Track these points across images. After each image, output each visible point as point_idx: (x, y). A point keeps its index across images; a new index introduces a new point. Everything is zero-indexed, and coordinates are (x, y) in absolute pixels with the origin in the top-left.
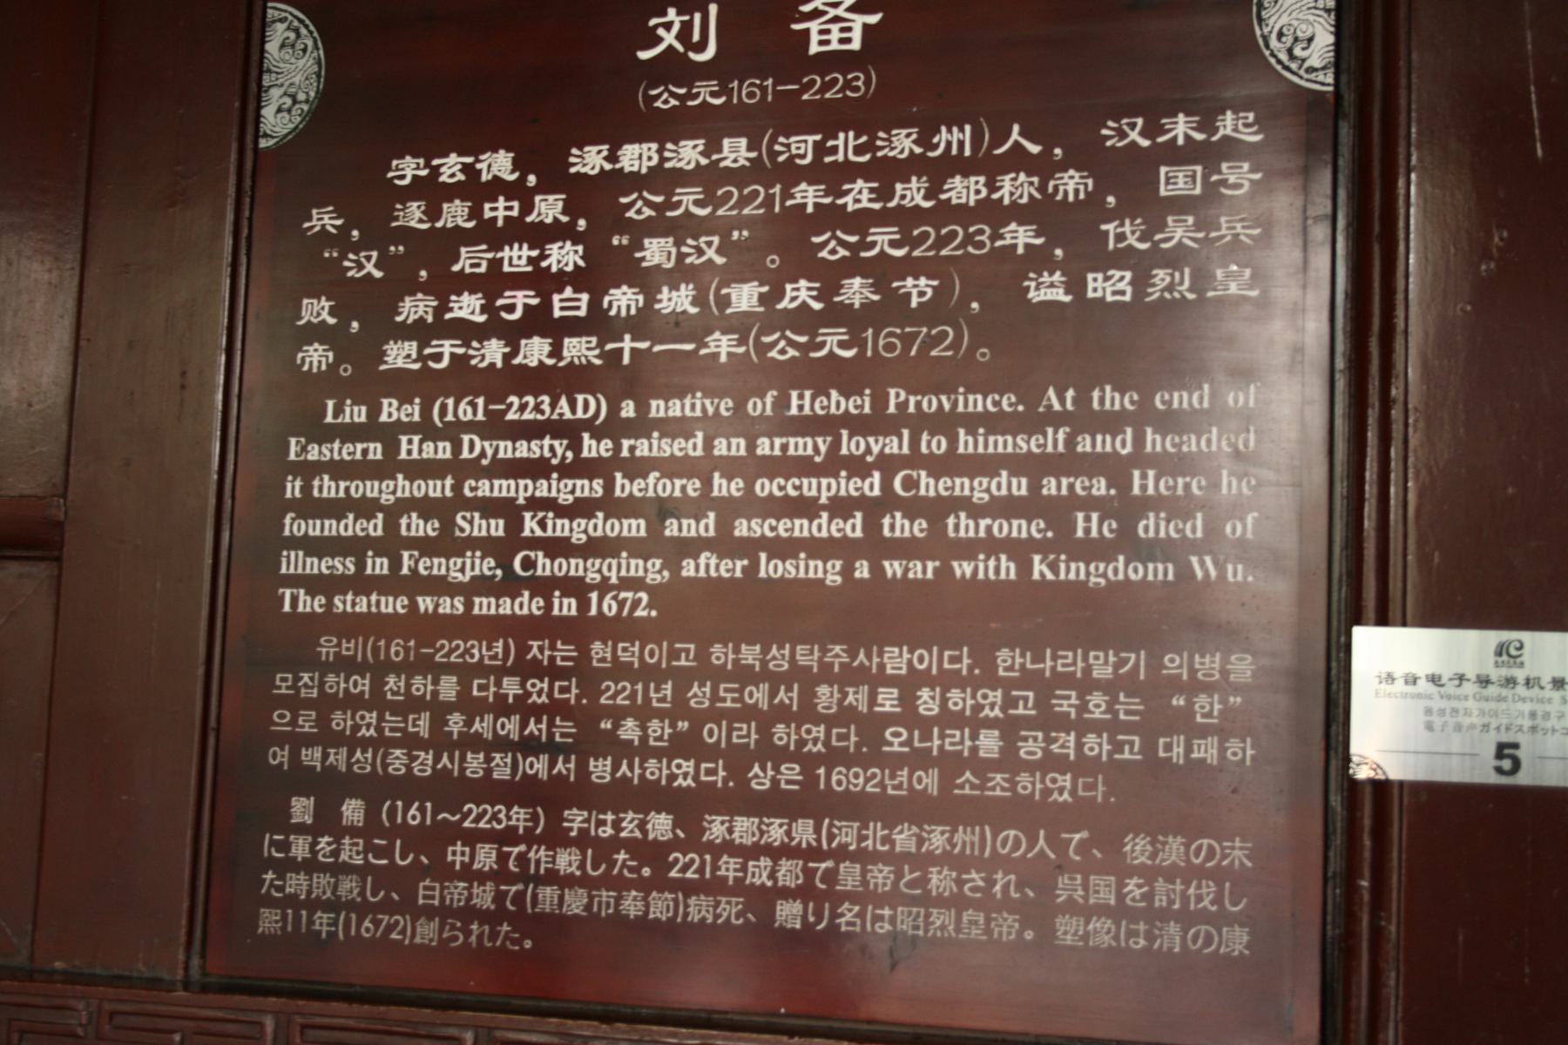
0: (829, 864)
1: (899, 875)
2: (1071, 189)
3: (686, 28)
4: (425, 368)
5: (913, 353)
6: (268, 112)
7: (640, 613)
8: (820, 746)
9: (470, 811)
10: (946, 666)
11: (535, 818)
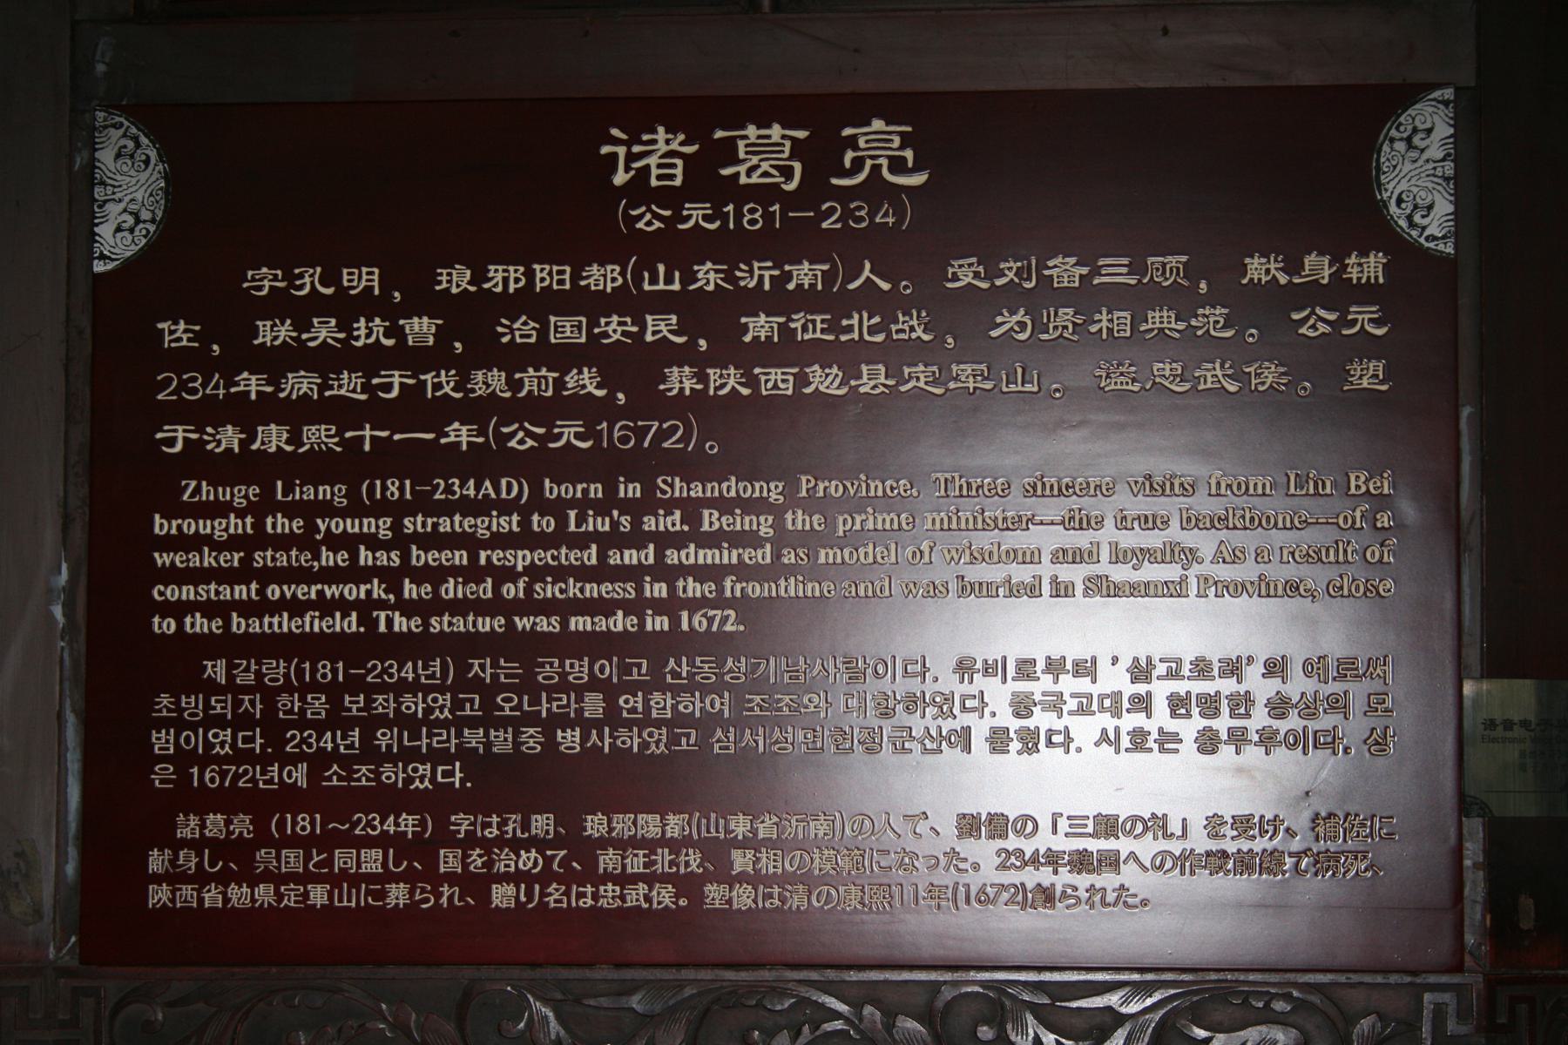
1: (308, 858)
4: (374, 397)
5: (646, 444)
6: (105, 231)
7: (729, 628)
9: (360, 820)
11: (422, 823)
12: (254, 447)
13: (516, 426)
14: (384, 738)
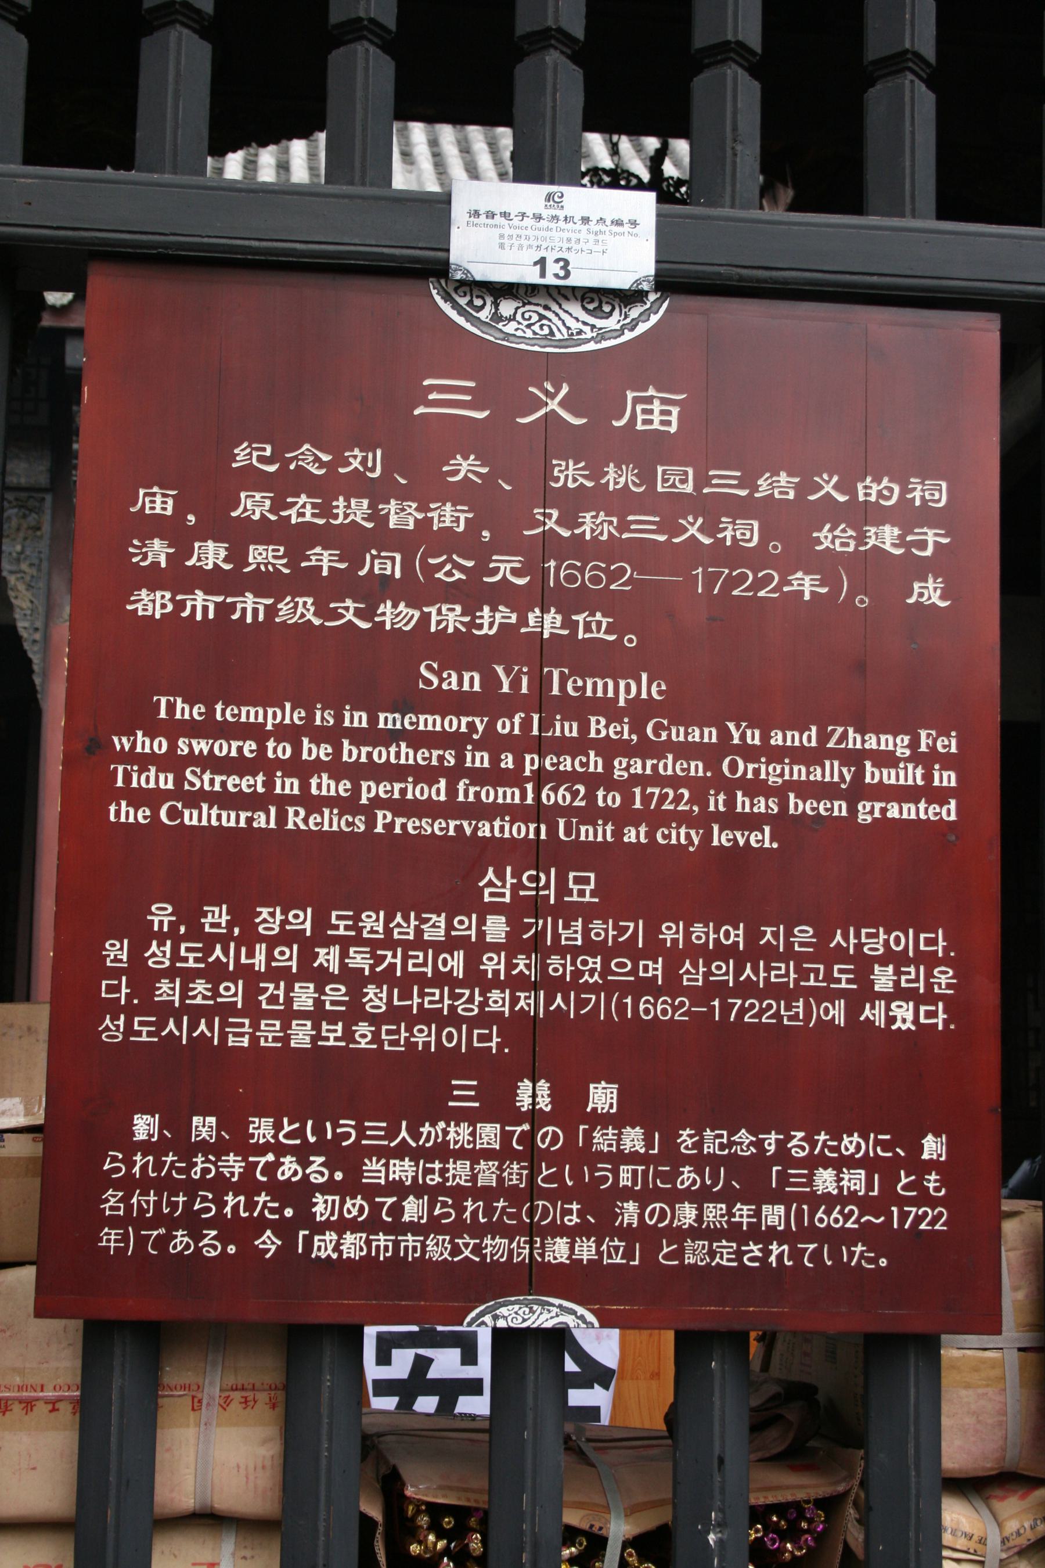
0: (270, 1157)
2: (199, 605)
3: (365, 460)
8: (596, 977)
10: (922, 947)
12: (189, 563)
13: (445, 557)
14: (375, 999)
